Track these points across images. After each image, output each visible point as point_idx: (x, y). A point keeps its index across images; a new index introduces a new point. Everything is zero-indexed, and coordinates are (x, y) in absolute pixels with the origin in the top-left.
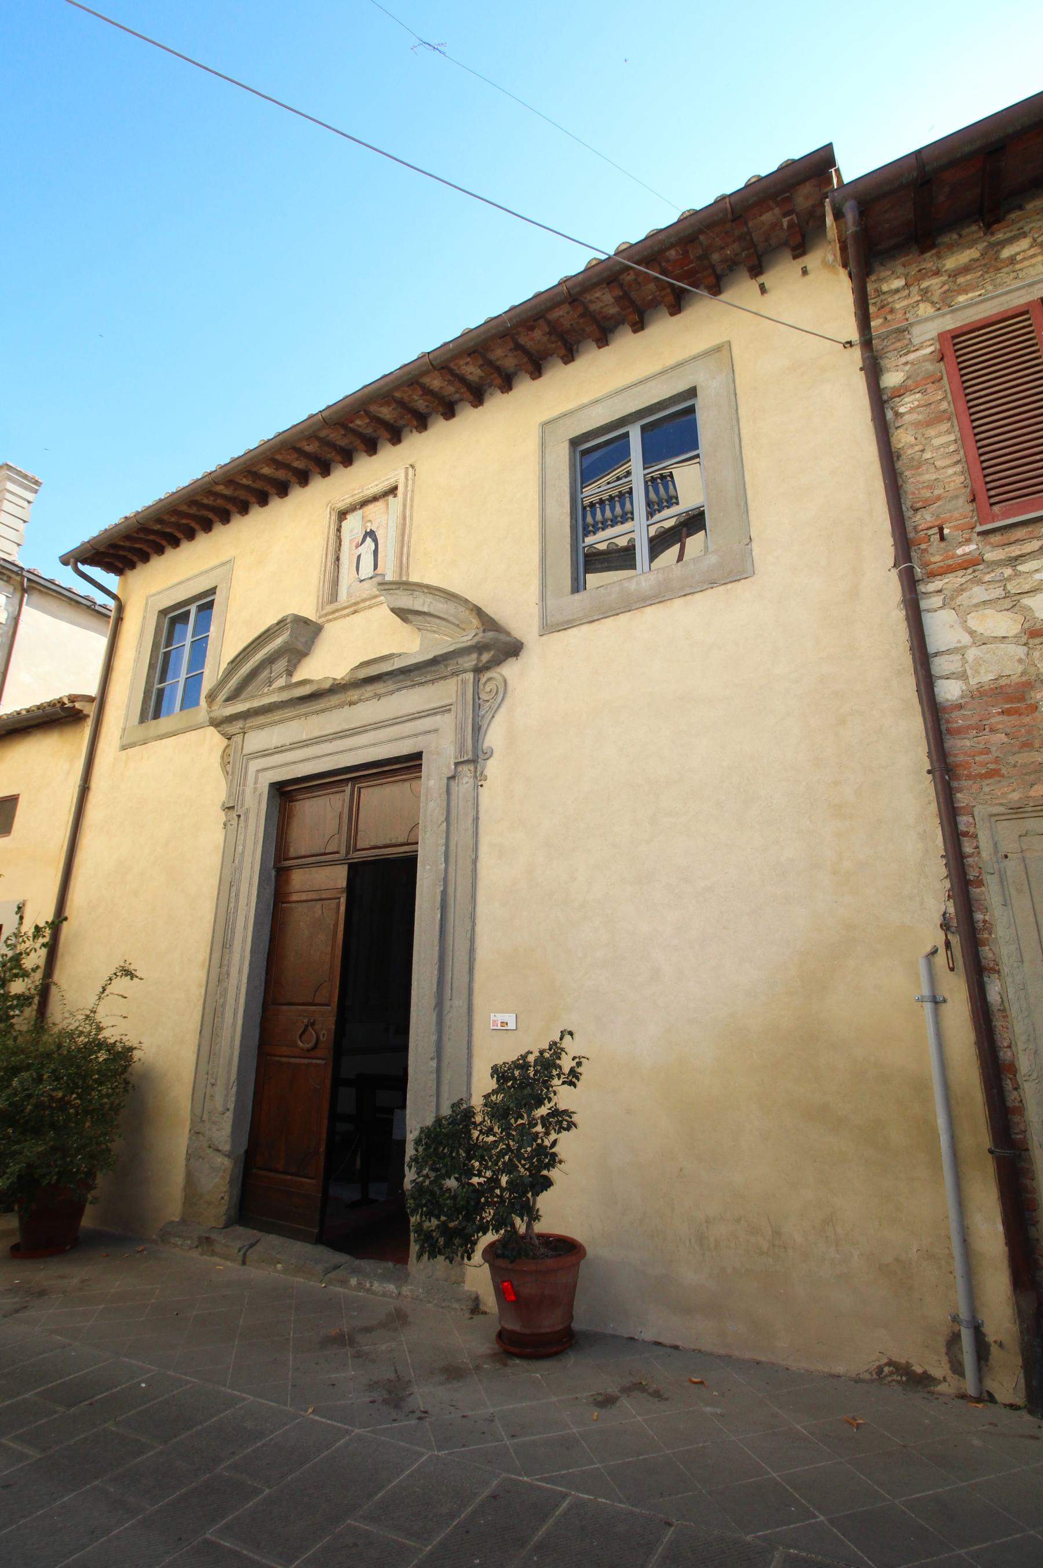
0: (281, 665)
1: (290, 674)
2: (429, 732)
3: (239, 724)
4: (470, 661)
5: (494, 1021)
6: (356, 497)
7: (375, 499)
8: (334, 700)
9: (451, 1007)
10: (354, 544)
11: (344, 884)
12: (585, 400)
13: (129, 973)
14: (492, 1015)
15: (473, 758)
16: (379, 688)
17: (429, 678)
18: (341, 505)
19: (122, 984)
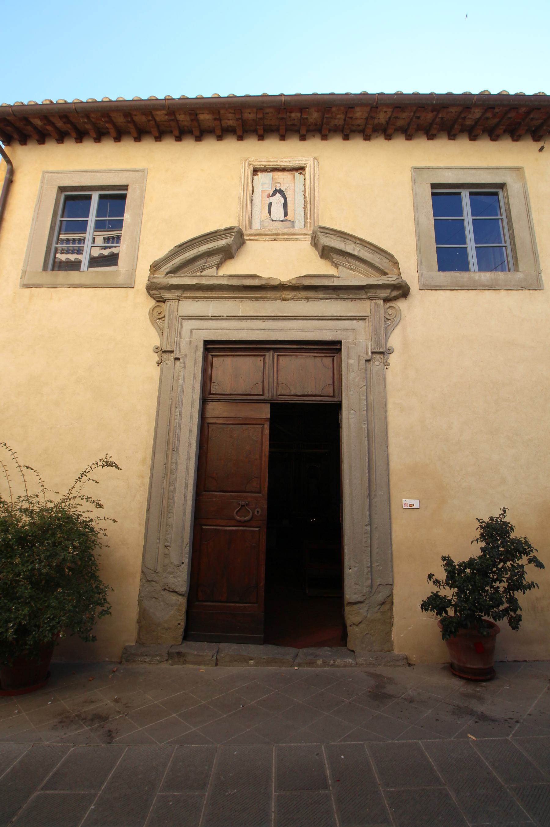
0: (216, 259)
1: (218, 266)
2: (347, 330)
3: (178, 293)
4: (385, 293)
5: (405, 504)
6: (271, 163)
7: (284, 170)
8: (270, 294)
9: (375, 495)
10: (266, 194)
11: (268, 416)
12: (441, 165)
13: (108, 464)
14: (403, 500)
15: (382, 353)
16: (311, 294)
17: (351, 296)
18: (258, 165)
19: (101, 472)
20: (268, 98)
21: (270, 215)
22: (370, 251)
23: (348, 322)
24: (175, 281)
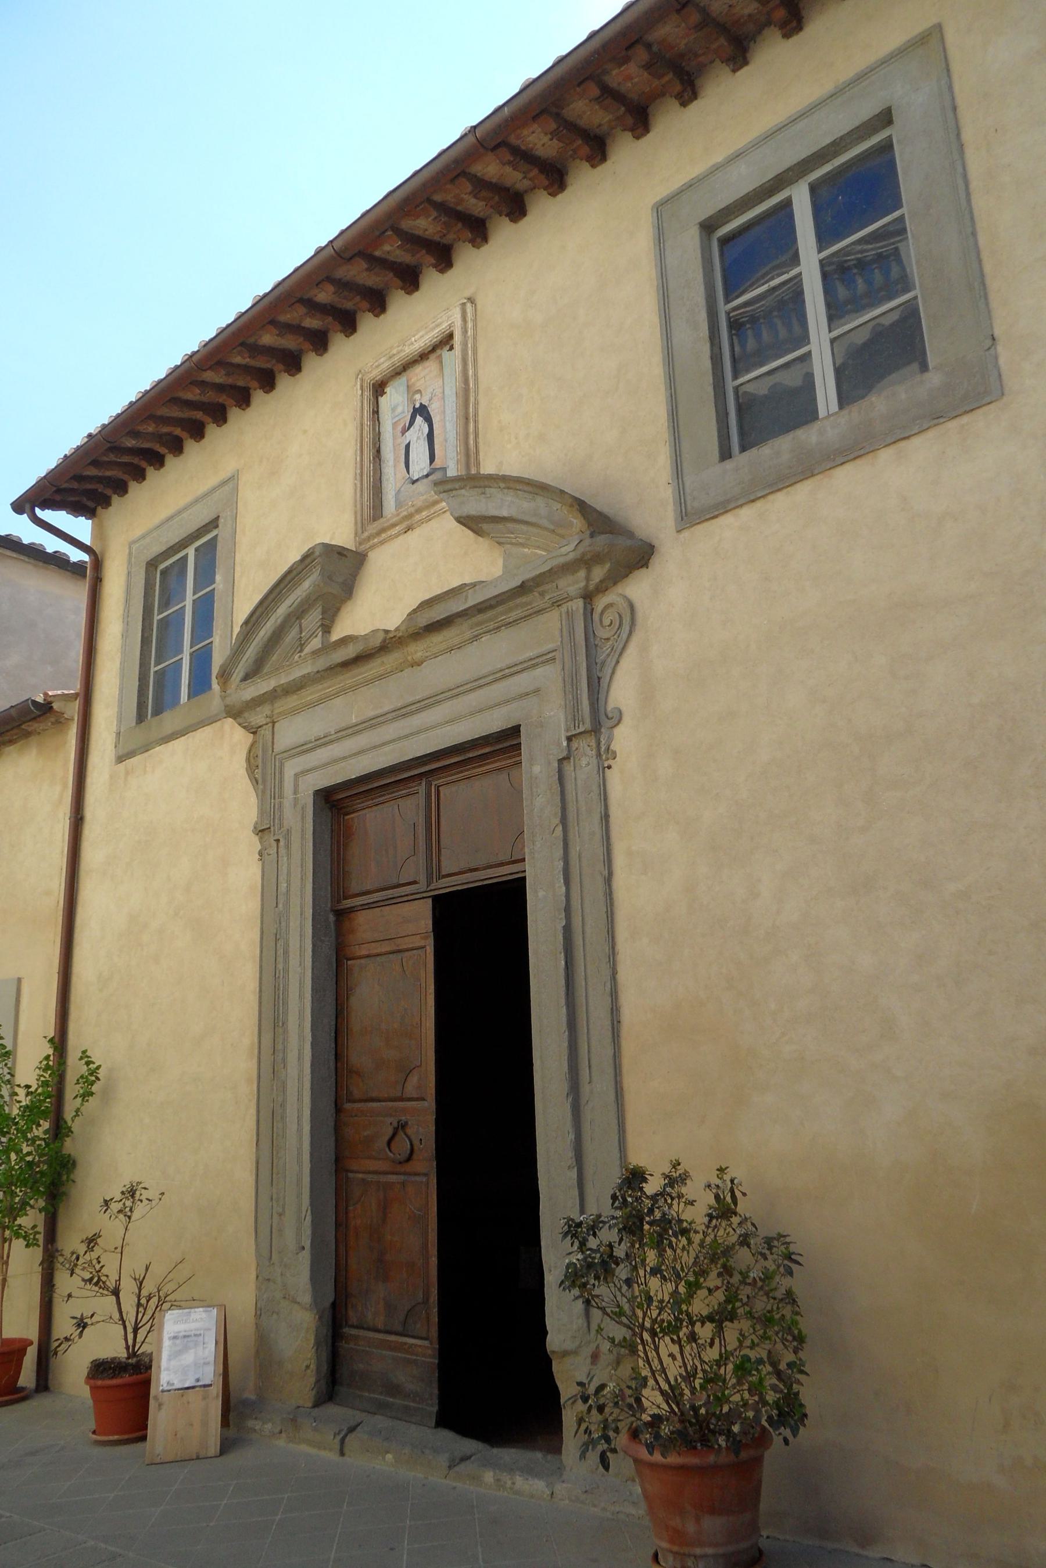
12: (718, 158)
20: (266, 301)
21: (408, 472)
22: (526, 495)
23: (495, 686)
24: (262, 686)
